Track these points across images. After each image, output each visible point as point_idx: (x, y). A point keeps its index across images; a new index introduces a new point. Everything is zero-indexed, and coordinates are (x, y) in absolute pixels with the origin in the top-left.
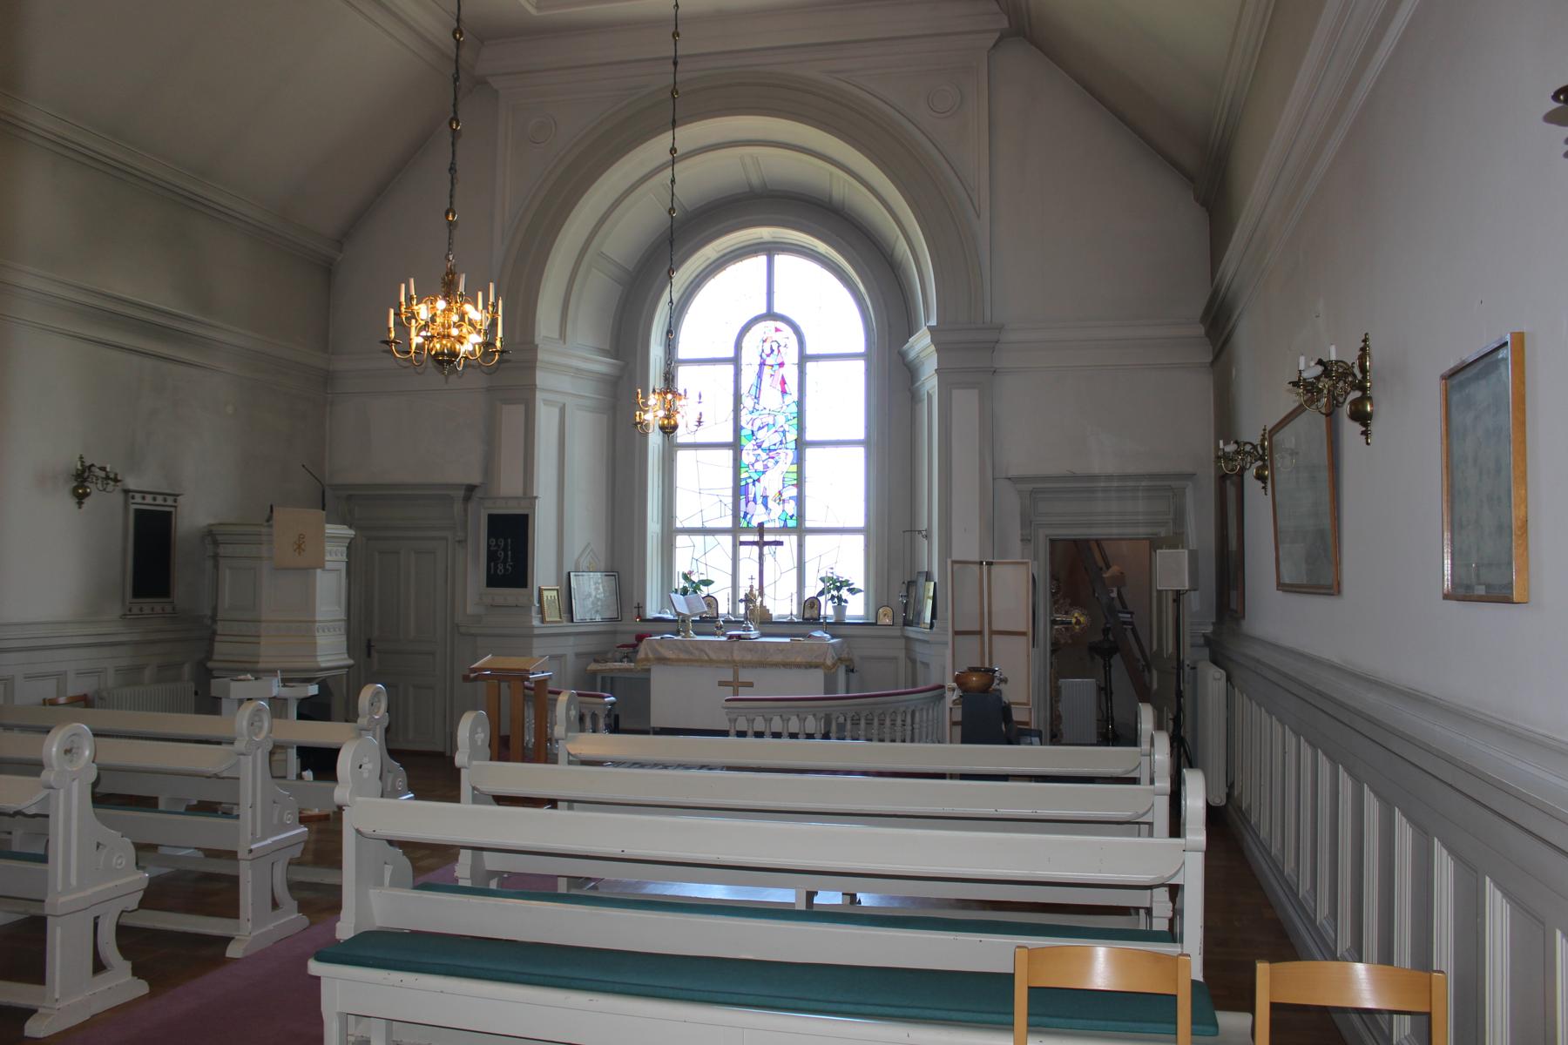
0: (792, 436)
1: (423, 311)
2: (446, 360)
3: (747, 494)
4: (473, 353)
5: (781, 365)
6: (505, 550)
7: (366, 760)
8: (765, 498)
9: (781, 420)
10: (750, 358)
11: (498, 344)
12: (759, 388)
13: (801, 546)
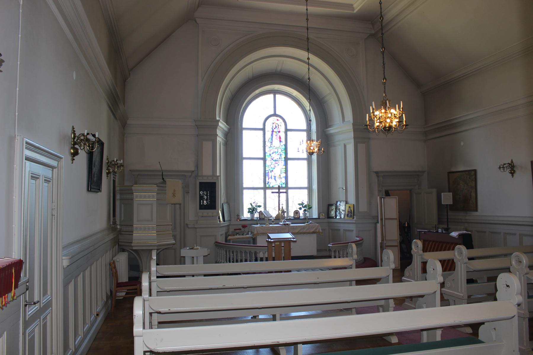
0: (283, 156)
1: (377, 113)
2: (388, 129)
3: (268, 175)
4: (396, 125)
5: (279, 132)
6: (207, 195)
7: (432, 272)
8: (275, 177)
9: (280, 151)
10: (268, 128)
11: (404, 123)
12: (272, 139)
13: (265, 193)
